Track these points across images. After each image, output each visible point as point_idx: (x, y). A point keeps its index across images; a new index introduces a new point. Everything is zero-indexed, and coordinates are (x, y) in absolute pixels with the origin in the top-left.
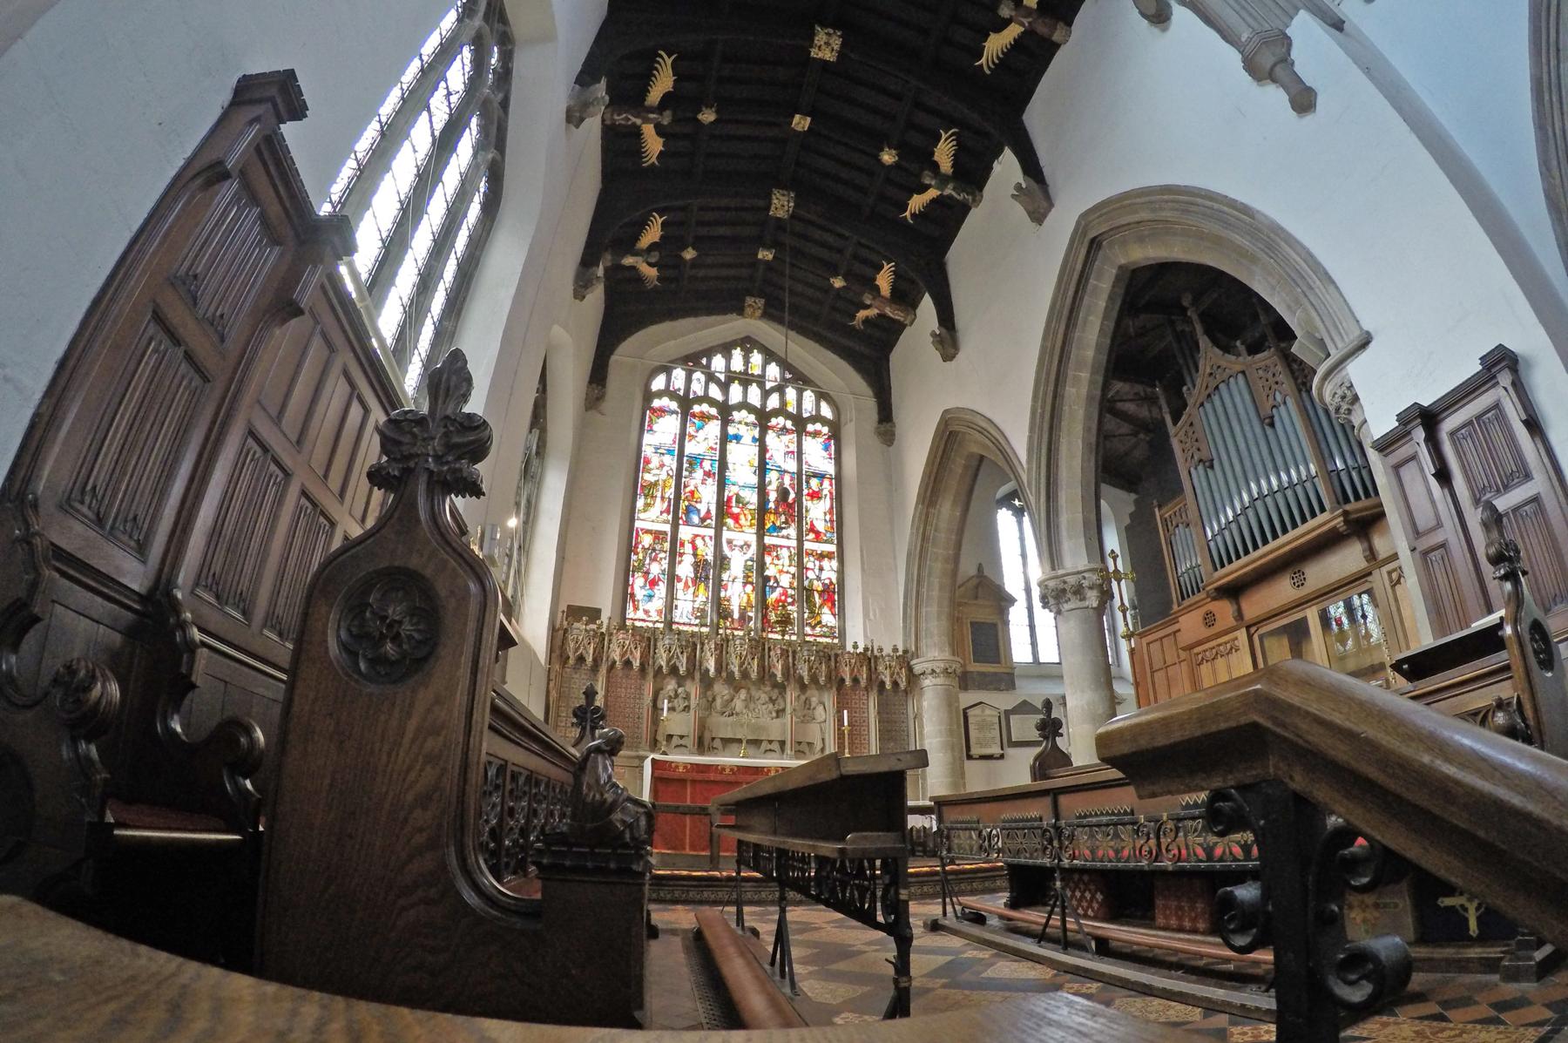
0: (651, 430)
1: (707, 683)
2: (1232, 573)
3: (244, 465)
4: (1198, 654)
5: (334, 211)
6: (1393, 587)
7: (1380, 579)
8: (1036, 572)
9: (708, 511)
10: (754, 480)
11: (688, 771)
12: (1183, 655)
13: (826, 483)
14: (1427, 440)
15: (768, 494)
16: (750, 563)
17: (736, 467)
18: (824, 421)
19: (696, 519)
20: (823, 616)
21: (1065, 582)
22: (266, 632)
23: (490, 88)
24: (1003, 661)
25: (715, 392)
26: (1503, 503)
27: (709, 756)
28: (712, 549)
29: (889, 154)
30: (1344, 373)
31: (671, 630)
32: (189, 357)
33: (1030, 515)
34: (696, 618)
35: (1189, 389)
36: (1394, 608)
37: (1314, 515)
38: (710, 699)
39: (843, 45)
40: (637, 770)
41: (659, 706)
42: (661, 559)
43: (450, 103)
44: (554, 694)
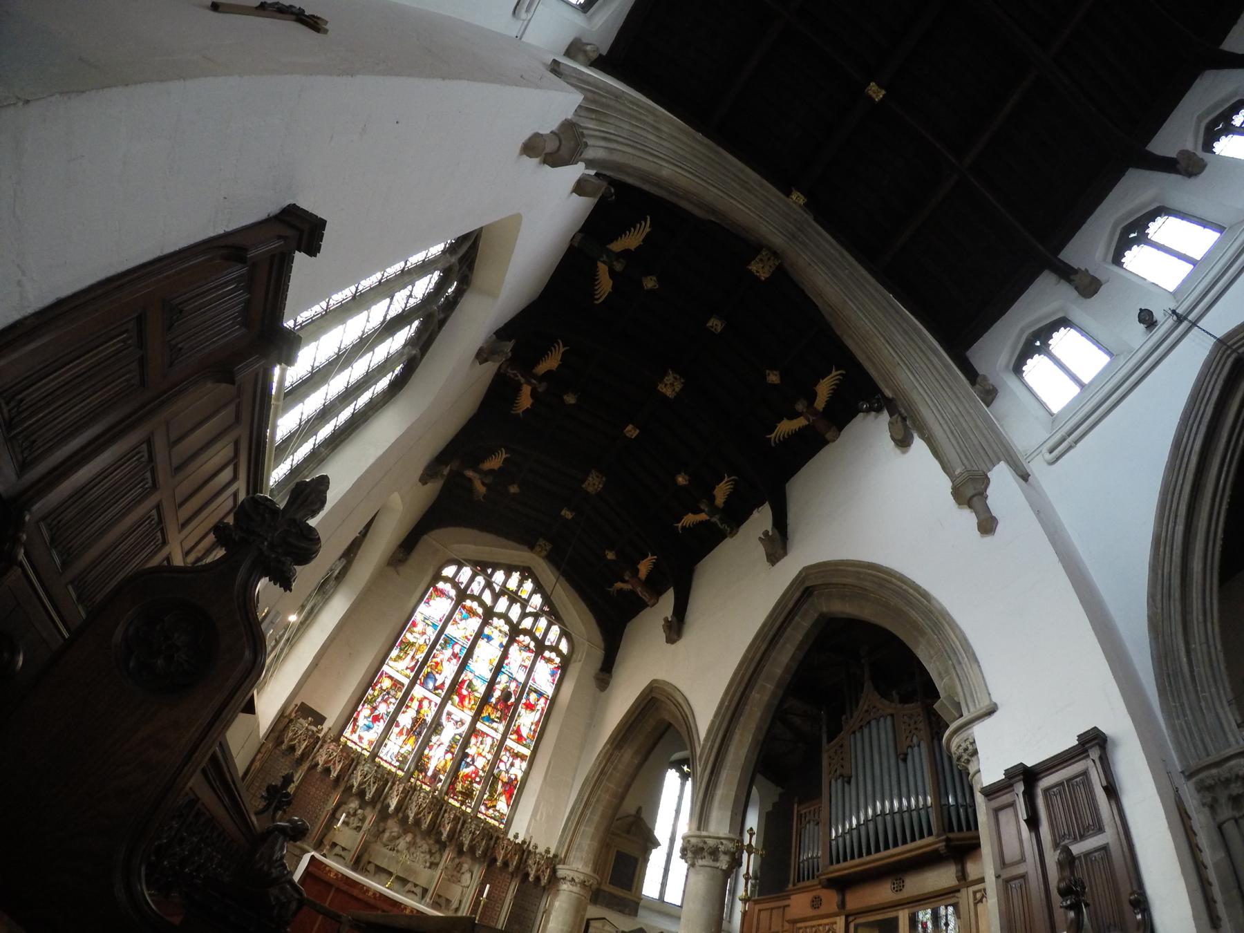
0: (428, 603)
1: (384, 815)
2: (845, 869)
3: (129, 460)
4: (800, 928)
5: (294, 328)
6: (976, 904)
7: (966, 896)
8: (684, 828)
9: (443, 684)
10: (488, 676)
11: (337, 879)
12: (787, 926)
13: (542, 700)
14: (1024, 793)
15: (494, 691)
16: (458, 737)
17: (479, 660)
18: (559, 653)
19: (431, 685)
20: (499, 803)
21: (705, 843)
22: (70, 588)
23: (438, 307)
24: (634, 890)
25: (487, 597)
26: (1076, 849)
27: (361, 875)
28: (434, 713)
29: (683, 478)
30: (970, 731)
31: (373, 760)
32: (142, 362)
33: (693, 781)
34: (398, 761)
35: (847, 719)
36: (973, 921)
37: (922, 836)
38: (381, 829)
39: (682, 390)
40: (296, 858)
41: (337, 815)
42: (391, 703)
43: (407, 302)
44: (257, 764)
